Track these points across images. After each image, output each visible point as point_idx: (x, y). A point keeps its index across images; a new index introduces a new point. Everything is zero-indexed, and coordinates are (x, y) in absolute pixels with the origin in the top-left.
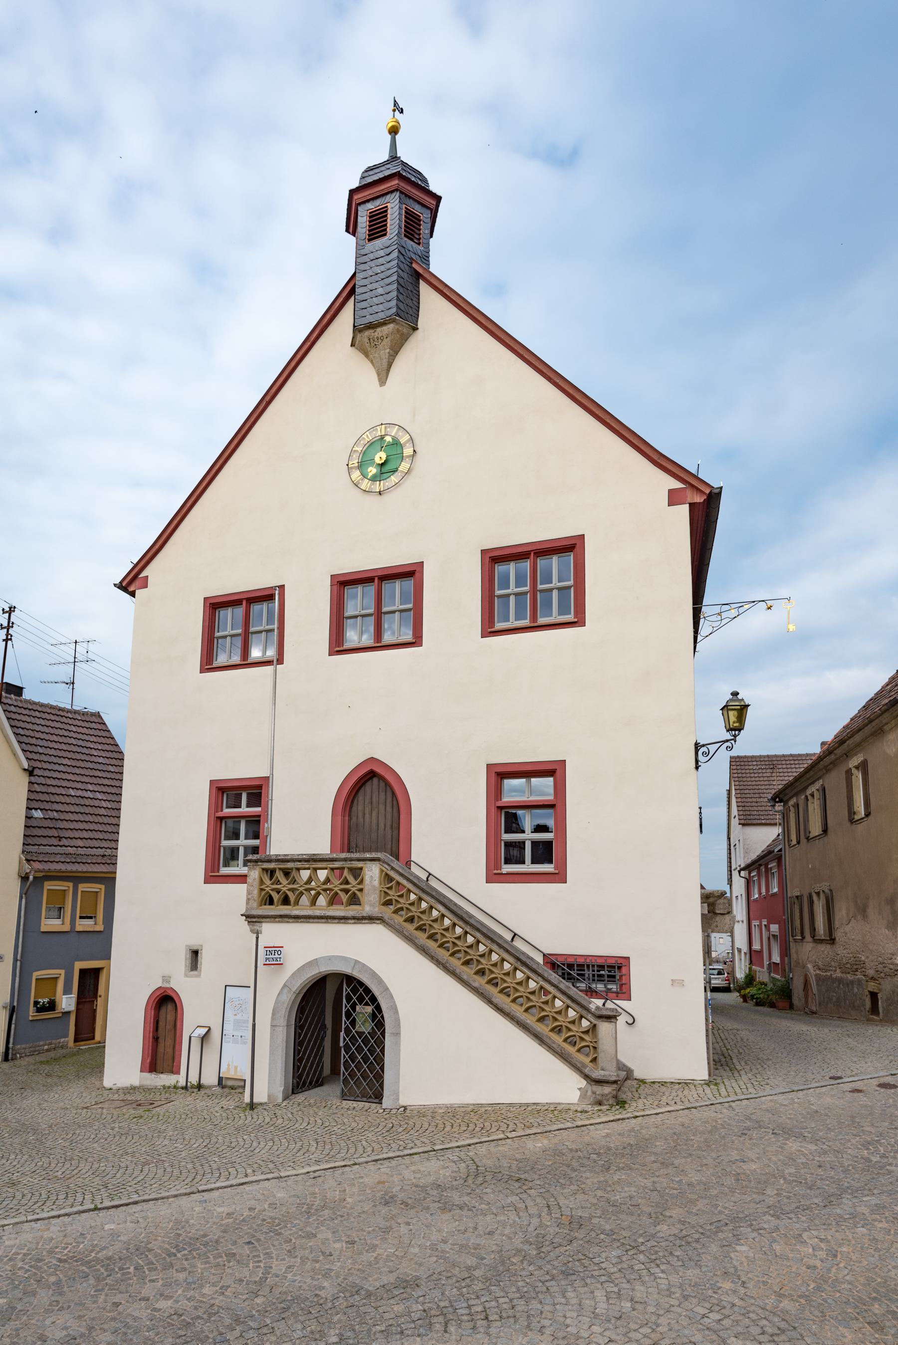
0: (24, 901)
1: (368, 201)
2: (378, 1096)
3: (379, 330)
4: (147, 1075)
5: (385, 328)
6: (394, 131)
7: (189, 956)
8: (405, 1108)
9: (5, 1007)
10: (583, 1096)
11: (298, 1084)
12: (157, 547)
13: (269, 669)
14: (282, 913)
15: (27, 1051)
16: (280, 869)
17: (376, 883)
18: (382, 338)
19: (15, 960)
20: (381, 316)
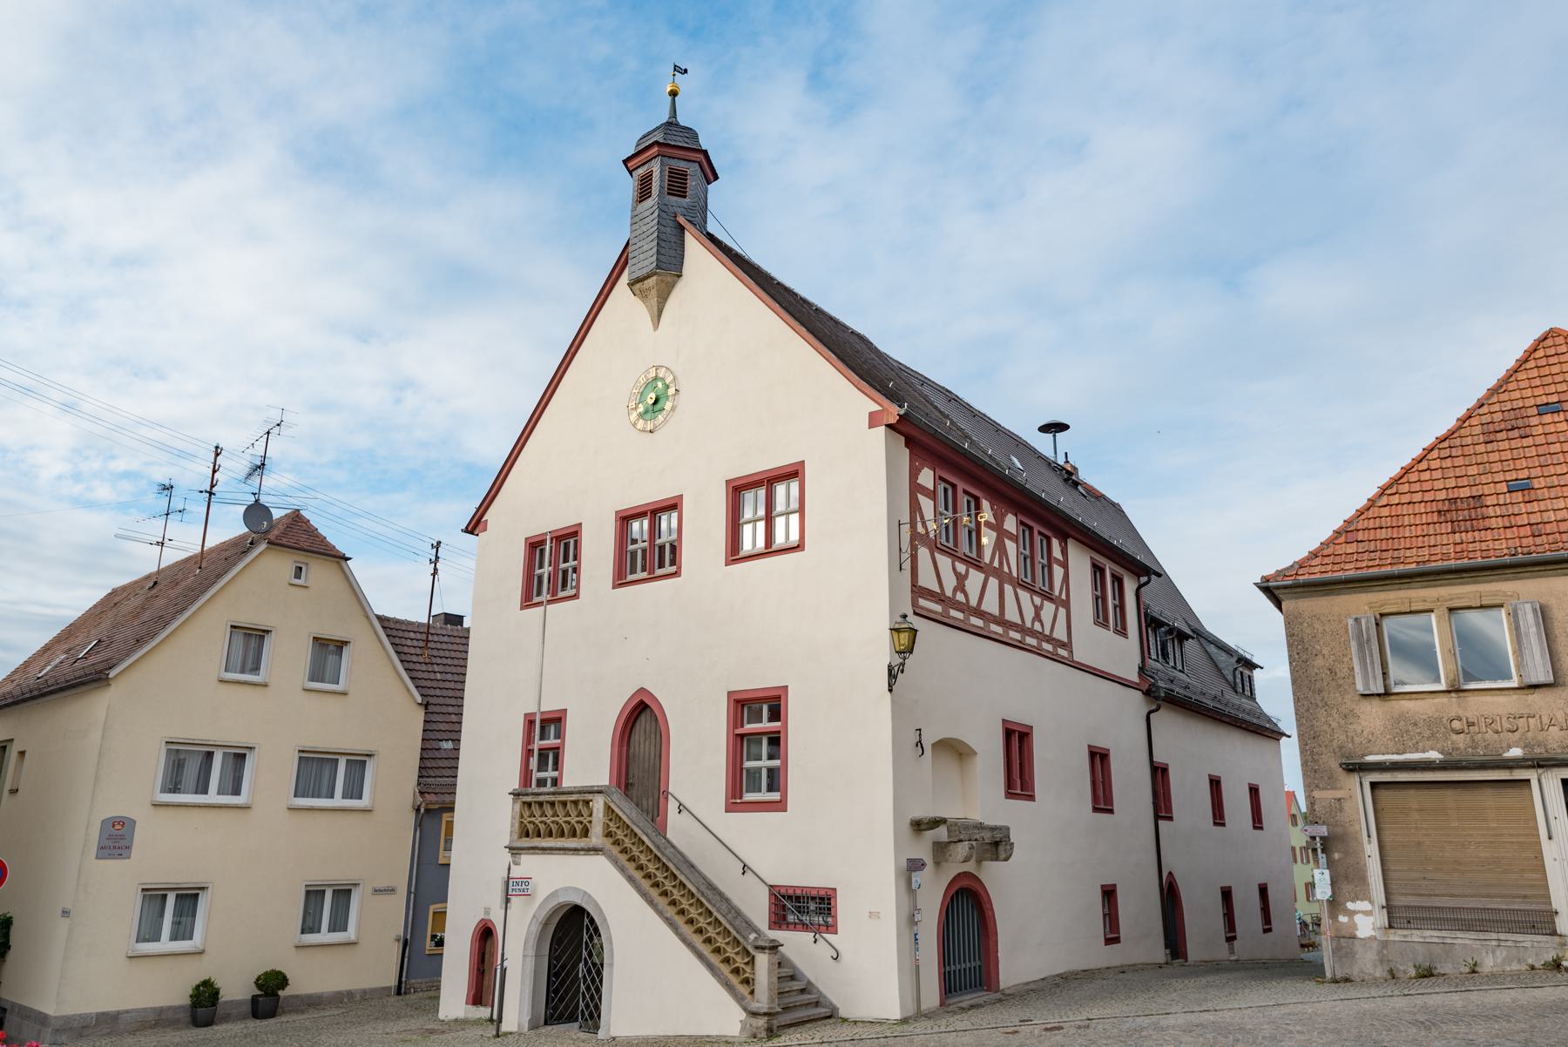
2: (597, 1027)
6: (674, 94)
10: (743, 1029)
17: (601, 815)
19: (409, 892)
20: (644, 271)
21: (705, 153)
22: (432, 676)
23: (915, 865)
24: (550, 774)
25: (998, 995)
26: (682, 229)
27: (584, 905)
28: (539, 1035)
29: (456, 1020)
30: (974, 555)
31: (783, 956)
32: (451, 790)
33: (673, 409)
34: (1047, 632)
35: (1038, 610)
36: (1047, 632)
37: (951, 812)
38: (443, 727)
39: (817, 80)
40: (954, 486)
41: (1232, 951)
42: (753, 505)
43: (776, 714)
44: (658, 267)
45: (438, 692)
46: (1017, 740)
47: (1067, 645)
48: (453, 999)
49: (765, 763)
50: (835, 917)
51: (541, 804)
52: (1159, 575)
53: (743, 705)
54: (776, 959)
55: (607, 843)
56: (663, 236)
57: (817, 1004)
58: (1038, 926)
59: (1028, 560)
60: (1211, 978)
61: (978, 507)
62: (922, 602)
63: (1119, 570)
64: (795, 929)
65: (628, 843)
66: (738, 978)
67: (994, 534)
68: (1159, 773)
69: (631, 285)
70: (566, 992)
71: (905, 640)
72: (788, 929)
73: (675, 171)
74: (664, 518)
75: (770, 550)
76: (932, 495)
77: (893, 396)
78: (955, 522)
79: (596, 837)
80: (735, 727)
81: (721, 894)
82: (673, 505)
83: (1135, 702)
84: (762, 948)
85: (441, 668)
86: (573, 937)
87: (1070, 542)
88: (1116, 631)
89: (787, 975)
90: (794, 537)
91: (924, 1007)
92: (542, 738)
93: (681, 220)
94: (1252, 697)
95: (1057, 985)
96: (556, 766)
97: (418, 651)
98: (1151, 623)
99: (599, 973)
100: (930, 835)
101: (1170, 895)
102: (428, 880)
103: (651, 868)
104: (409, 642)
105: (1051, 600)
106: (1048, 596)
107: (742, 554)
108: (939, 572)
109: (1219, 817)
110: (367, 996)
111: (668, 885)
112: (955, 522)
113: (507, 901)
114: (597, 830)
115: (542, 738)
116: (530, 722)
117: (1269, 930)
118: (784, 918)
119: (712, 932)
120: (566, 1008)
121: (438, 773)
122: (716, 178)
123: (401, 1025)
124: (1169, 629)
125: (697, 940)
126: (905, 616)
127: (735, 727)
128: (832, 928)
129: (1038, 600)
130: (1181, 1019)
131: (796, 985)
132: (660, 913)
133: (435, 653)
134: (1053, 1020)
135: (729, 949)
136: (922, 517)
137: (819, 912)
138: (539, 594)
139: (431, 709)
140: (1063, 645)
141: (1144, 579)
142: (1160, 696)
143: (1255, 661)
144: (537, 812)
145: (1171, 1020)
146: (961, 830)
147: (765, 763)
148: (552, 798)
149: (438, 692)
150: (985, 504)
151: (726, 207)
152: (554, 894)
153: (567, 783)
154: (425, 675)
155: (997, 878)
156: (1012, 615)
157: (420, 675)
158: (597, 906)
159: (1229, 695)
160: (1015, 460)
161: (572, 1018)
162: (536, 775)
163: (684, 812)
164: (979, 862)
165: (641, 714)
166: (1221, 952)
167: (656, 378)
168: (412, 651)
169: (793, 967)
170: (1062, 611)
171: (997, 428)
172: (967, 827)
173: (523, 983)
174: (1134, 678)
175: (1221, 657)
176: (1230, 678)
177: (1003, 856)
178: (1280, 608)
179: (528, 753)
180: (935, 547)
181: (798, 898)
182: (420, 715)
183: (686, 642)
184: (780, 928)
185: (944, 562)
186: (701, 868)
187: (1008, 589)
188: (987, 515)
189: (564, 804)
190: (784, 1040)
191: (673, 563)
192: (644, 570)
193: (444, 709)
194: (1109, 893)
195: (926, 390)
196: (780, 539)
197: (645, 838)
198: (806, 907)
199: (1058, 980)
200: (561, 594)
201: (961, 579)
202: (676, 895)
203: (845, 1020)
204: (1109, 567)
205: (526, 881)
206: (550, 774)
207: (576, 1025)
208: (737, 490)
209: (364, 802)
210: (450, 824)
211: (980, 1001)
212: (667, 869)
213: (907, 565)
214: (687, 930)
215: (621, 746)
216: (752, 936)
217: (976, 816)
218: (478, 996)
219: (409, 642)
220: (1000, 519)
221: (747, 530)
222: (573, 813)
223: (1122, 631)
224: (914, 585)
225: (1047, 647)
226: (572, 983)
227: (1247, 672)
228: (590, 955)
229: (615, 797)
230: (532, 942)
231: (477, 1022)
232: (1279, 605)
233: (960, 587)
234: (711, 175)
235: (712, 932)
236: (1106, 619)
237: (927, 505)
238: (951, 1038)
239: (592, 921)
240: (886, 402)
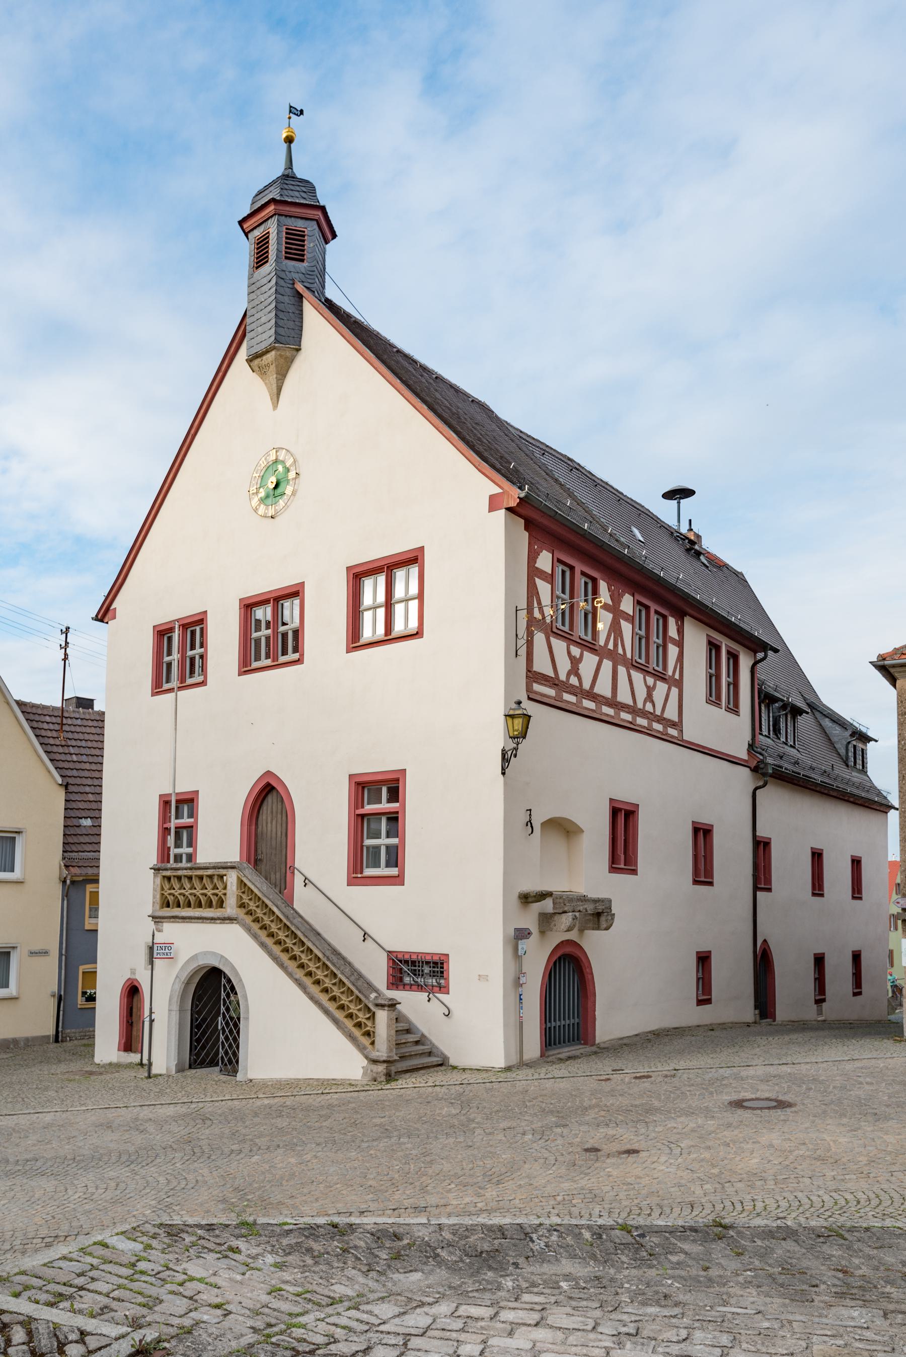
0: (65, 902)
1: (255, 228)
2: (235, 1072)
3: (264, 358)
4: (122, 1053)
6: (289, 140)
8: (251, 1081)
9: (54, 996)
10: (365, 1074)
11: (195, 1061)
12: (120, 580)
13: (172, 695)
14: (174, 914)
15: (77, 1035)
16: (185, 876)
17: (235, 888)
18: (268, 365)
19: (61, 955)
21: (323, 209)
22: (68, 758)
23: (521, 934)
24: (185, 850)
25: (594, 1049)
26: (300, 297)
27: (221, 967)
28: (185, 1077)
29: (110, 1064)
30: (589, 638)
31: (400, 1012)
32: (95, 863)
33: (294, 493)
35: (650, 690)
36: (658, 712)
37: (558, 884)
38: (81, 805)
39: (434, 84)
40: (572, 568)
41: (820, 1012)
42: (373, 591)
43: (395, 794)
44: (277, 341)
45: (75, 773)
46: (623, 818)
48: (107, 1046)
49: (384, 841)
50: (447, 980)
51: (179, 878)
52: (776, 651)
53: (364, 787)
54: (394, 1015)
55: (240, 913)
56: (281, 306)
57: (430, 1054)
58: (632, 984)
59: (643, 640)
60: (794, 1036)
61: (595, 592)
62: (537, 687)
63: (735, 646)
64: (411, 990)
65: (259, 913)
66: (360, 1030)
67: (610, 616)
68: (761, 847)
69: (249, 361)
70: (207, 1041)
71: (519, 725)
72: (404, 989)
73: (291, 227)
74: (287, 604)
75: (389, 638)
76: (550, 578)
77: (513, 477)
78: (572, 607)
79: (231, 906)
80: (356, 808)
81: (344, 959)
82: (296, 592)
83: (743, 778)
84: (382, 1006)
85: (76, 750)
87: (687, 620)
88: (728, 709)
89: (404, 1029)
90: (413, 624)
91: (526, 1057)
92: (177, 818)
93: (300, 287)
94: (864, 770)
95: (649, 1040)
96: (191, 844)
97: (55, 734)
98: (764, 698)
99: (236, 1025)
100: (536, 907)
101: (763, 961)
102: (78, 945)
103: (282, 935)
104: (45, 726)
105: (663, 679)
106: (661, 677)
107: (363, 641)
109: (818, 888)
110: (29, 1043)
111: (297, 951)
112: (572, 607)
113: (151, 963)
114: (231, 902)
115: (177, 818)
116: (165, 803)
117: (860, 993)
118: (401, 979)
119: (336, 991)
120: (207, 1055)
121: (79, 848)
122: (334, 236)
123: (63, 1067)
124: (784, 707)
125: (324, 998)
126: (519, 703)
127: (356, 808)
128: (444, 989)
129: (650, 681)
130: (760, 1071)
131: (411, 1038)
132: (290, 975)
133: (70, 735)
134: (643, 1070)
135: (352, 1006)
136: (539, 603)
137: (433, 974)
138: (168, 681)
139: (71, 788)
140: (674, 725)
141: (760, 655)
142: (767, 772)
143: (870, 734)
144: (176, 885)
145: (751, 1072)
146: (565, 903)
147: (384, 841)
148: (189, 873)
149: (75, 773)
150: (603, 586)
151: (349, 272)
152: (194, 958)
153: (202, 858)
154: (63, 757)
155: (598, 947)
156: (624, 696)
157: (58, 757)
158: (233, 968)
159: (841, 770)
160: (636, 532)
161: (213, 1063)
162: (174, 851)
163: (309, 886)
164: (581, 931)
165: (267, 795)
166: (810, 1012)
167: (276, 461)
168: (49, 734)
169: (408, 1021)
170: (675, 691)
171: (619, 497)
172: (571, 900)
173: (169, 1033)
174: (743, 754)
175: (835, 731)
176: (842, 751)
177: (604, 924)
178: (895, 686)
179: (165, 831)
180: (551, 632)
181: (413, 963)
182: (61, 795)
183: (309, 726)
184: (397, 989)
185: (559, 646)
186: (325, 935)
187: (622, 670)
188: (604, 596)
189: (201, 878)
190: (401, 1083)
191: (296, 650)
192: (268, 657)
193: (82, 789)
194: (704, 959)
195: (546, 460)
196: (399, 627)
197: (275, 909)
198: (421, 971)
199: (650, 1036)
200: (190, 681)
201: (575, 662)
202: (304, 959)
203: (454, 1068)
204: (725, 644)
205: (168, 946)
206: (185, 850)
207: (217, 1069)
208: (357, 576)
209: (16, 875)
210: (95, 896)
211: (578, 1053)
212: (296, 936)
213: (523, 651)
214: (315, 990)
215: (250, 825)
216: (373, 995)
218: (129, 1042)
219: (45, 726)
220: (616, 599)
221: (367, 616)
222: (209, 886)
223: (734, 709)
224: (529, 670)
225: (657, 727)
226: (212, 1034)
227: (860, 746)
228: (228, 1009)
229: (247, 872)
231: (130, 1066)
232: (893, 681)
233: (574, 670)
234: (329, 233)
235: (336, 991)
236: (719, 697)
237: (544, 588)
238: (549, 1084)
239: (229, 981)
240: (507, 485)
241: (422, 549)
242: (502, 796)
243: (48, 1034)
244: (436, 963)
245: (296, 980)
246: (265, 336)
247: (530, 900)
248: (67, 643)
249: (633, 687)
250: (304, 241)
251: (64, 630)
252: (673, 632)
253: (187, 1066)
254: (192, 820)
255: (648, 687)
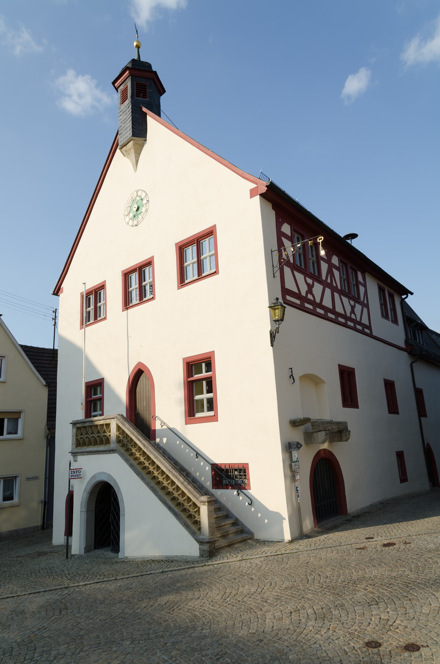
0: (48, 448)
3: (128, 145)
5: (130, 144)
7: (394, 458)
9: (42, 502)
14: (83, 451)
16: (89, 426)
17: (115, 431)
34: (358, 319)
35: (353, 308)
43: (209, 366)
44: (133, 135)
47: (369, 327)
59: (346, 280)
68: (419, 393)
83: (404, 358)
86: (105, 502)
88: (392, 321)
97: (49, 362)
108: (297, 282)
152: (94, 476)
155: (343, 453)
156: (339, 309)
169: (228, 510)
170: (365, 310)
174: (403, 345)
177: (344, 439)
194: (400, 455)
198: (230, 477)
201: (310, 288)
205: (79, 470)
207: (110, 548)
208: (181, 249)
213: (278, 274)
217: (327, 416)
219: (45, 358)
223: (395, 321)
230: (84, 504)
241: (215, 226)
242: (273, 360)
243: (37, 525)
244: (240, 470)
245: (151, 487)
246: (127, 134)
247: (297, 424)
248: (56, 317)
249: (343, 305)
250: (146, 89)
251: (54, 310)
252: (360, 279)
253: (93, 547)
254: (101, 395)
255: (351, 306)
